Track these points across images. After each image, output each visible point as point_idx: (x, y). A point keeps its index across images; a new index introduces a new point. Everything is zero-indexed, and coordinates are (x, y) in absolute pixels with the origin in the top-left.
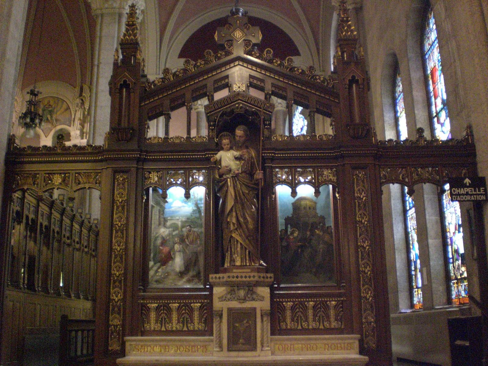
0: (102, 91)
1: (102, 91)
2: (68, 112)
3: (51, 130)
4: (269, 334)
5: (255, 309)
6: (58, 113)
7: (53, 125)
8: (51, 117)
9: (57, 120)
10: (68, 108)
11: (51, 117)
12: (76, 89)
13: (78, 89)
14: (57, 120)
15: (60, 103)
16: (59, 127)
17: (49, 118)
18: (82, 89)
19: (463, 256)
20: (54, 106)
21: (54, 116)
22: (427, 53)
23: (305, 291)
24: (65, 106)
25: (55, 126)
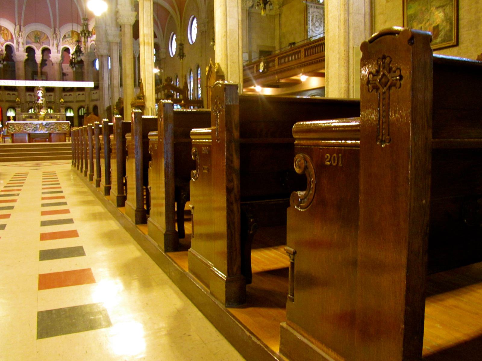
0: (211, 237)
1: (211, 237)
2: (48, 39)
3: (40, 47)
4: (326, 87)
5: (151, 115)
6: (43, 39)
7: (41, 44)
8: (40, 41)
9: (43, 43)
10: (47, 37)
11: (40, 41)
12: (52, 30)
13: (52, 30)
14: (43, 43)
15: (43, 35)
16: (44, 46)
17: (39, 41)
18: (55, 30)
19: (136, 113)
20: (40, 36)
21: (41, 41)
22: (441, 30)
23: (24, 152)
24: (46, 36)
25: (42, 45)
